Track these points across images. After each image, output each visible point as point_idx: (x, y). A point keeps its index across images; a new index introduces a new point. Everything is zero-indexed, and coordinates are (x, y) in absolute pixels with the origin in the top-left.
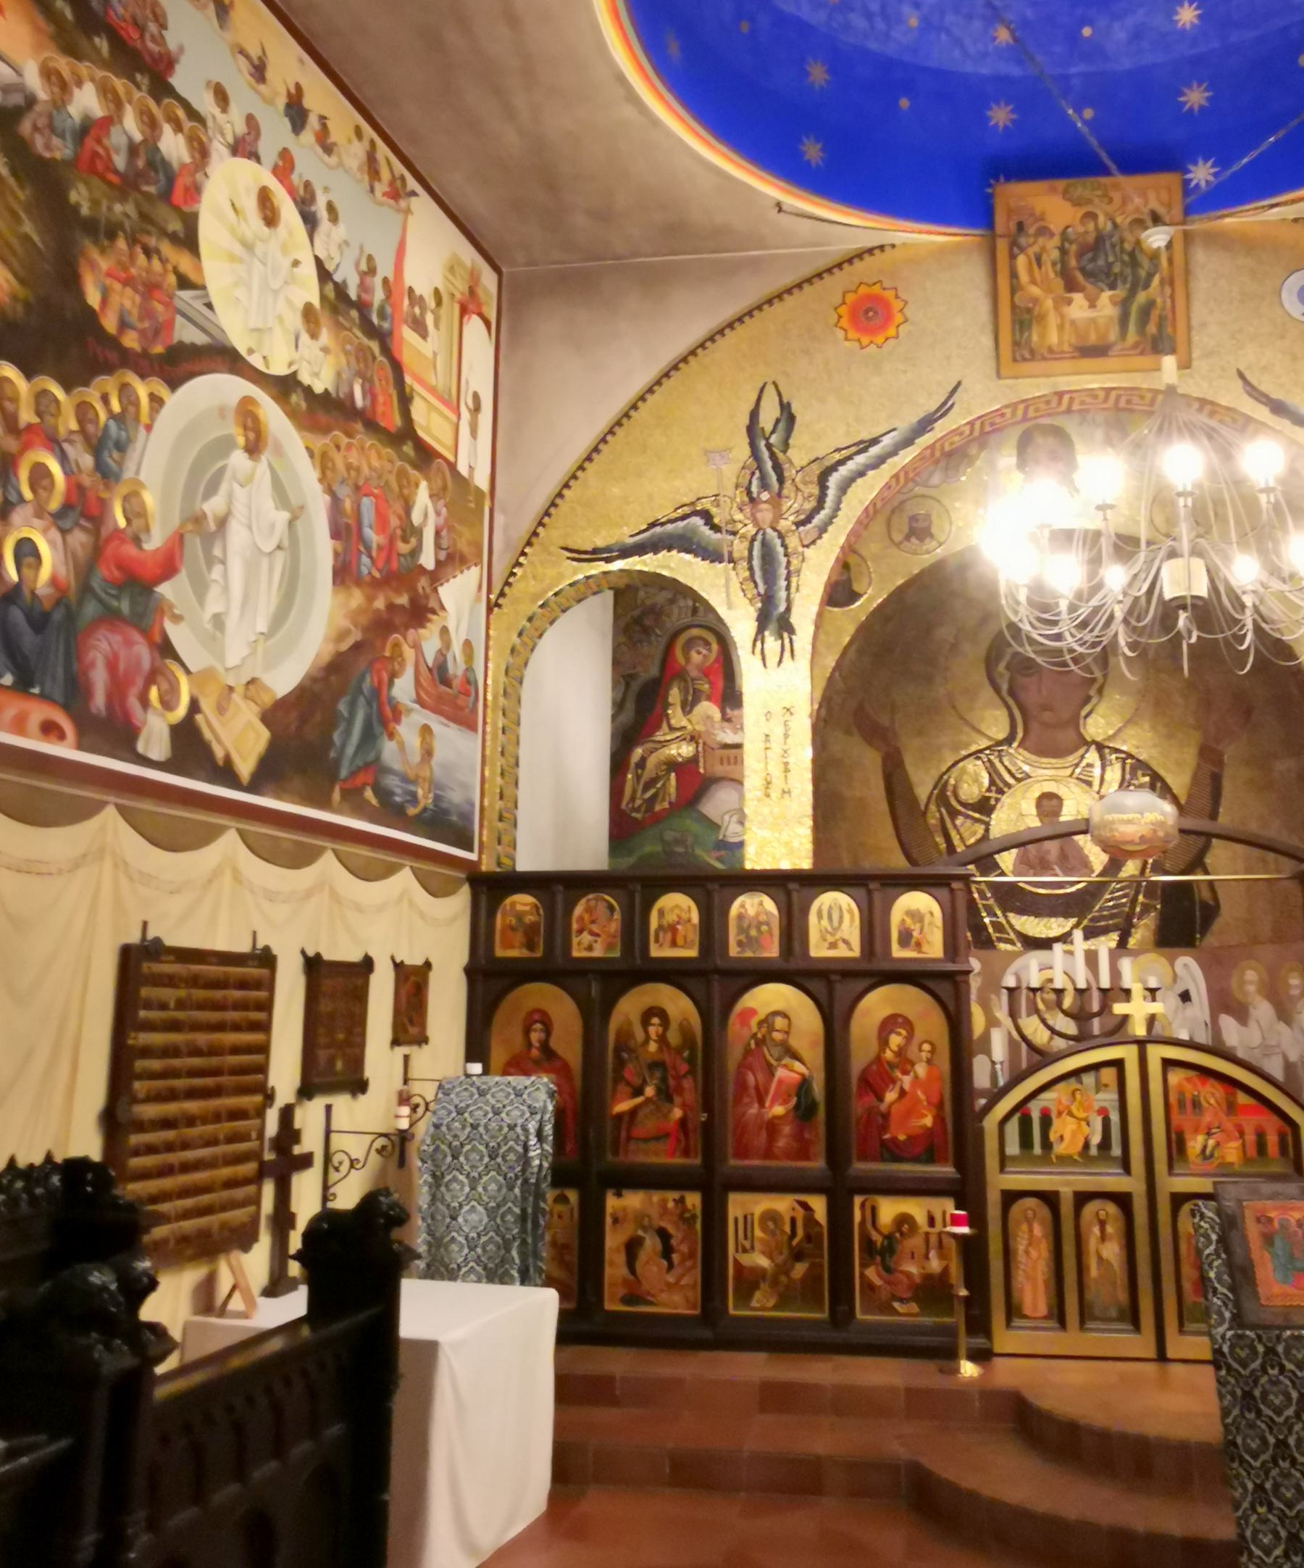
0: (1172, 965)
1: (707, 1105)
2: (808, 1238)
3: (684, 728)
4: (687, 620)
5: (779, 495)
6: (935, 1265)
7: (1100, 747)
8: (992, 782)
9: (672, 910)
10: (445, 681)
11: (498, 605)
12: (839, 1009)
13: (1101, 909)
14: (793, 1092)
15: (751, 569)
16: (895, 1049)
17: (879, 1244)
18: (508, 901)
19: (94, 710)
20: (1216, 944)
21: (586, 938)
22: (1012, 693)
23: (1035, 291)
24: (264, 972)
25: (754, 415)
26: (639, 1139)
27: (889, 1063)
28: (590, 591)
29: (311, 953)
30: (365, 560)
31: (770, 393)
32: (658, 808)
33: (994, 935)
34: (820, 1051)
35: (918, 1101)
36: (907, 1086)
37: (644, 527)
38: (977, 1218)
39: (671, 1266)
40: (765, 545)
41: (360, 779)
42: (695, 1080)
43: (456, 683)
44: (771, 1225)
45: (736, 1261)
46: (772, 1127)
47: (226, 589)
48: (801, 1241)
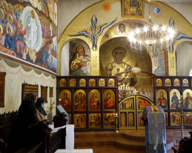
2: (98, 118)
4: (79, 45)
5: (95, 29)
6: (113, 120)
7: (124, 63)
8: (112, 67)
10: (54, 51)
11: (59, 42)
15: (92, 39)
18: (61, 80)
19: (18, 52)
21: (71, 84)
23: (127, 6)
24: (37, 88)
25: (92, 19)
29: (42, 85)
30: (45, 34)
31: (94, 16)
34: (100, 97)
39: (82, 122)
40: (93, 36)
41: (46, 63)
43: (55, 52)
46: (94, 106)
47: (31, 37)
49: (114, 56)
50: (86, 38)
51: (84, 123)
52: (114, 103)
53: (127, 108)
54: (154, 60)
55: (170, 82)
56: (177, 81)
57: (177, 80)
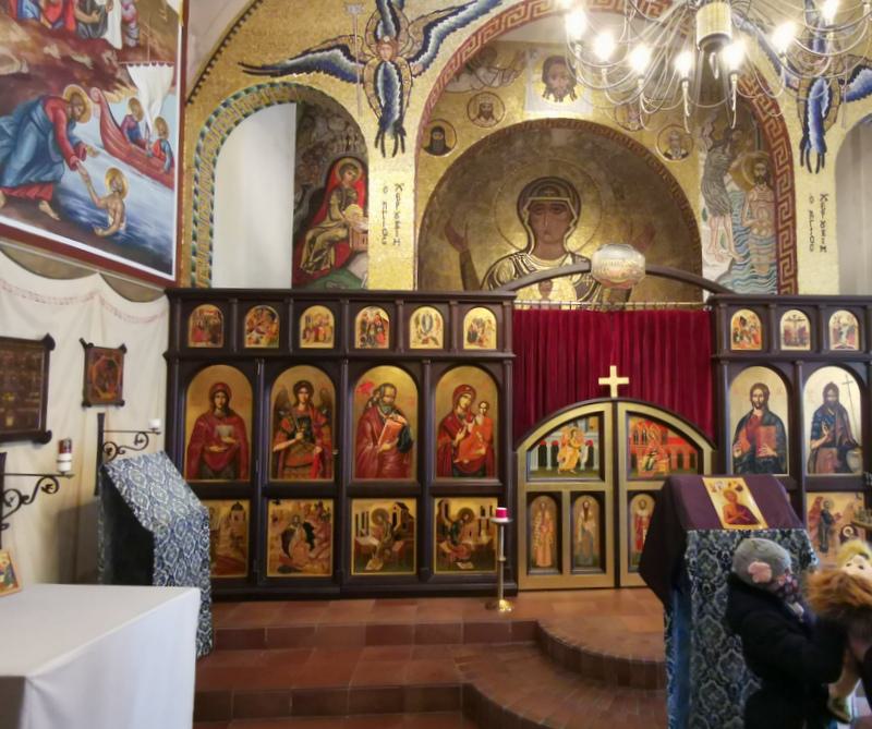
2: (404, 526)
3: (339, 220)
5: (396, 38)
6: (484, 539)
7: (573, 255)
9: (316, 316)
11: (190, 101)
14: (397, 434)
16: (463, 406)
18: (198, 309)
21: (255, 335)
22: (530, 224)
26: (291, 467)
27: (459, 416)
28: (263, 103)
32: (323, 268)
36: (470, 430)
37: (299, 53)
38: (513, 514)
39: (312, 547)
42: (331, 429)
44: (380, 519)
46: (382, 457)
49: (526, 223)
50: (344, 83)
53: (562, 471)
54: (712, 230)
55: (804, 329)
56: (845, 325)
57: (842, 319)
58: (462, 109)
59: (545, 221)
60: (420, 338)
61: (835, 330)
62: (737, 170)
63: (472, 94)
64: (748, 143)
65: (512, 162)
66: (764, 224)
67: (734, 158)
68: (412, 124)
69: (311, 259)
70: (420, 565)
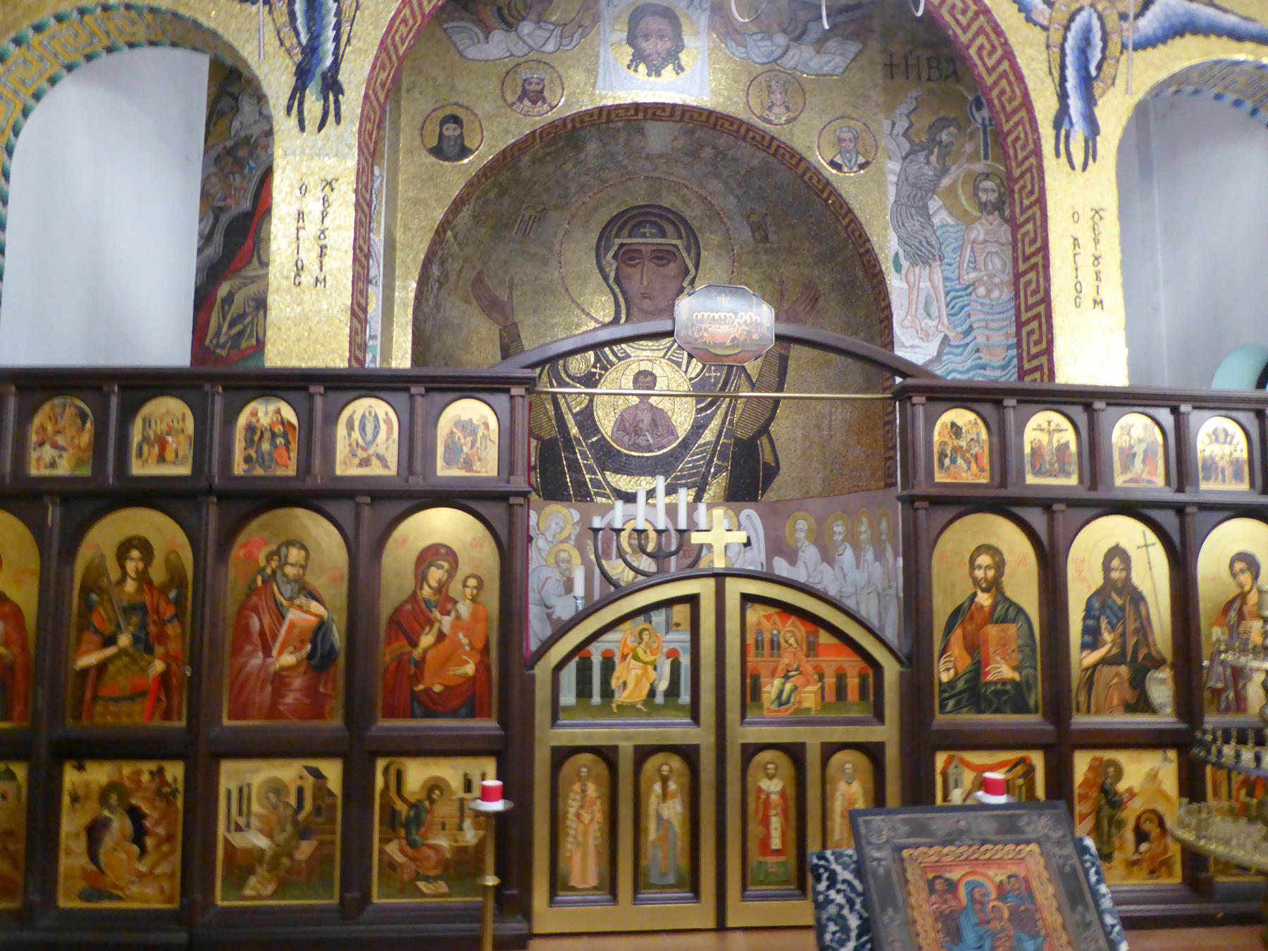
0: (738, 515)
1: (195, 658)
2: (317, 810)
12: (365, 539)
13: (682, 470)
14: (310, 636)
16: (434, 584)
17: (404, 814)
20: (775, 499)
33: (592, 491)
35: (461, 645)
36: (446, 629)
45: (226, 840)
46: (279, 680)
48: (309, 815)
49: (611, 281)
51: (165, 856)
52: (486, 650)
53: (620, 707)
54: (910, 288)
55: (1066, 445)
56: (1140, 441)
58: (493, 86)
59: (642, 277)
60: (354, 455)
61: (1121, 450)
62: (951, 190)
63: (510, 63)
64: (969, 148)
65: (584, 179)
66: (997, 280)
67: (945, 171)
68: (355, 75)
69: (225, 329)
70: (345, 887)
